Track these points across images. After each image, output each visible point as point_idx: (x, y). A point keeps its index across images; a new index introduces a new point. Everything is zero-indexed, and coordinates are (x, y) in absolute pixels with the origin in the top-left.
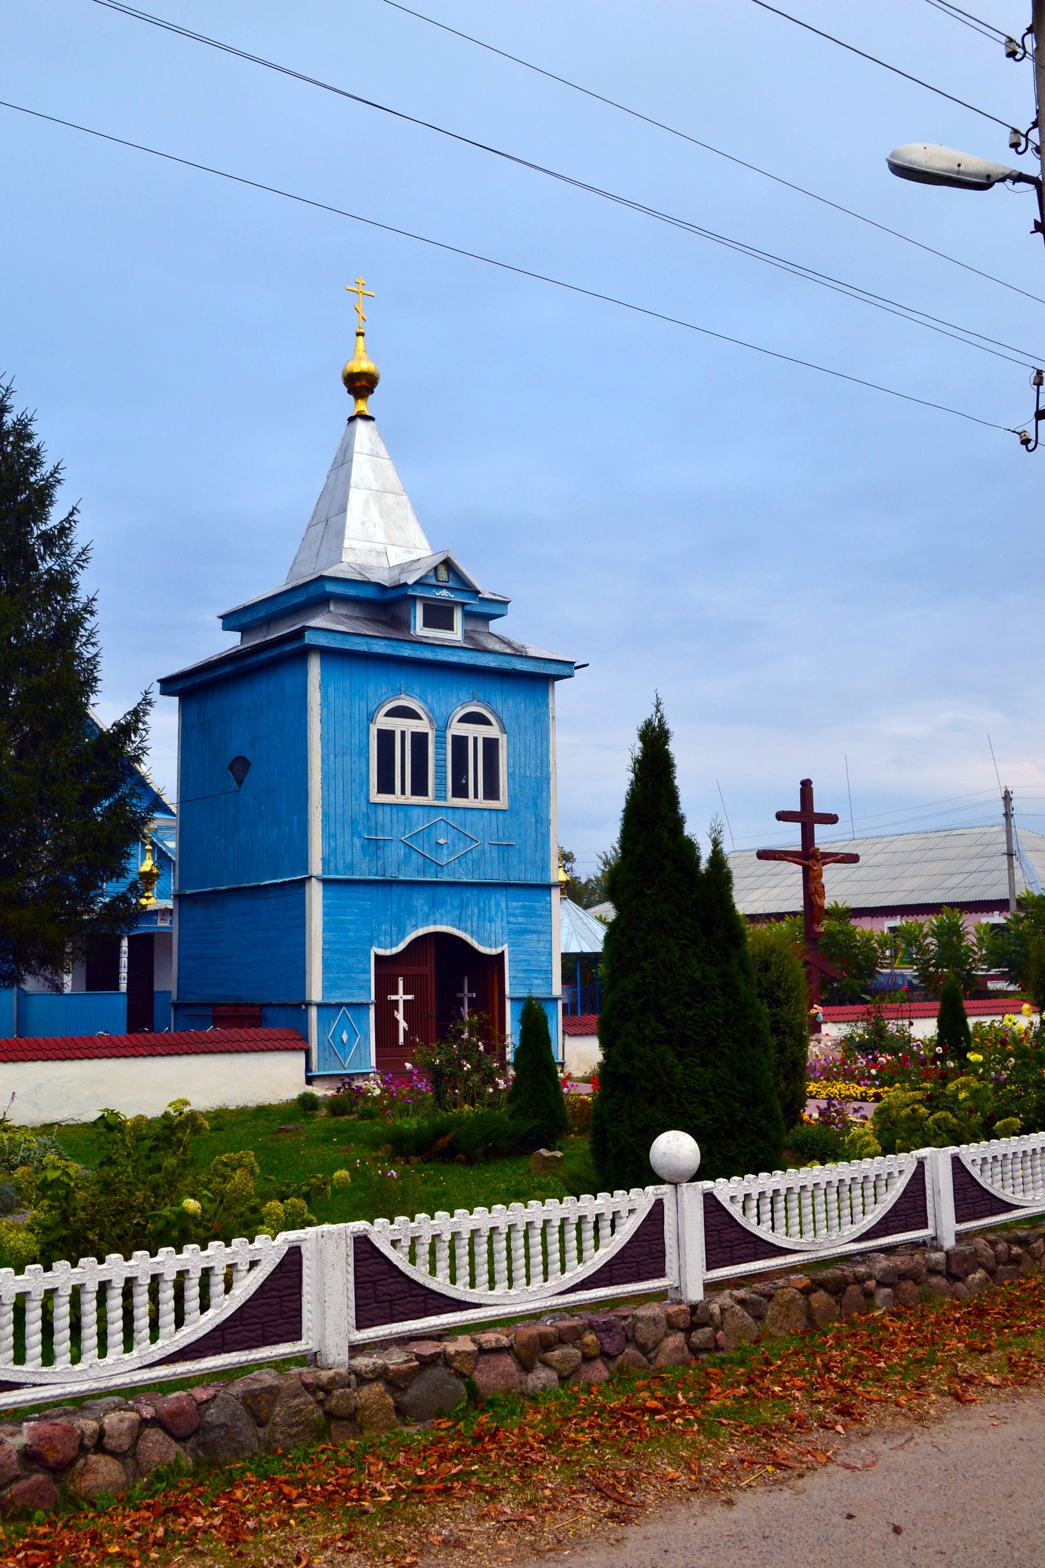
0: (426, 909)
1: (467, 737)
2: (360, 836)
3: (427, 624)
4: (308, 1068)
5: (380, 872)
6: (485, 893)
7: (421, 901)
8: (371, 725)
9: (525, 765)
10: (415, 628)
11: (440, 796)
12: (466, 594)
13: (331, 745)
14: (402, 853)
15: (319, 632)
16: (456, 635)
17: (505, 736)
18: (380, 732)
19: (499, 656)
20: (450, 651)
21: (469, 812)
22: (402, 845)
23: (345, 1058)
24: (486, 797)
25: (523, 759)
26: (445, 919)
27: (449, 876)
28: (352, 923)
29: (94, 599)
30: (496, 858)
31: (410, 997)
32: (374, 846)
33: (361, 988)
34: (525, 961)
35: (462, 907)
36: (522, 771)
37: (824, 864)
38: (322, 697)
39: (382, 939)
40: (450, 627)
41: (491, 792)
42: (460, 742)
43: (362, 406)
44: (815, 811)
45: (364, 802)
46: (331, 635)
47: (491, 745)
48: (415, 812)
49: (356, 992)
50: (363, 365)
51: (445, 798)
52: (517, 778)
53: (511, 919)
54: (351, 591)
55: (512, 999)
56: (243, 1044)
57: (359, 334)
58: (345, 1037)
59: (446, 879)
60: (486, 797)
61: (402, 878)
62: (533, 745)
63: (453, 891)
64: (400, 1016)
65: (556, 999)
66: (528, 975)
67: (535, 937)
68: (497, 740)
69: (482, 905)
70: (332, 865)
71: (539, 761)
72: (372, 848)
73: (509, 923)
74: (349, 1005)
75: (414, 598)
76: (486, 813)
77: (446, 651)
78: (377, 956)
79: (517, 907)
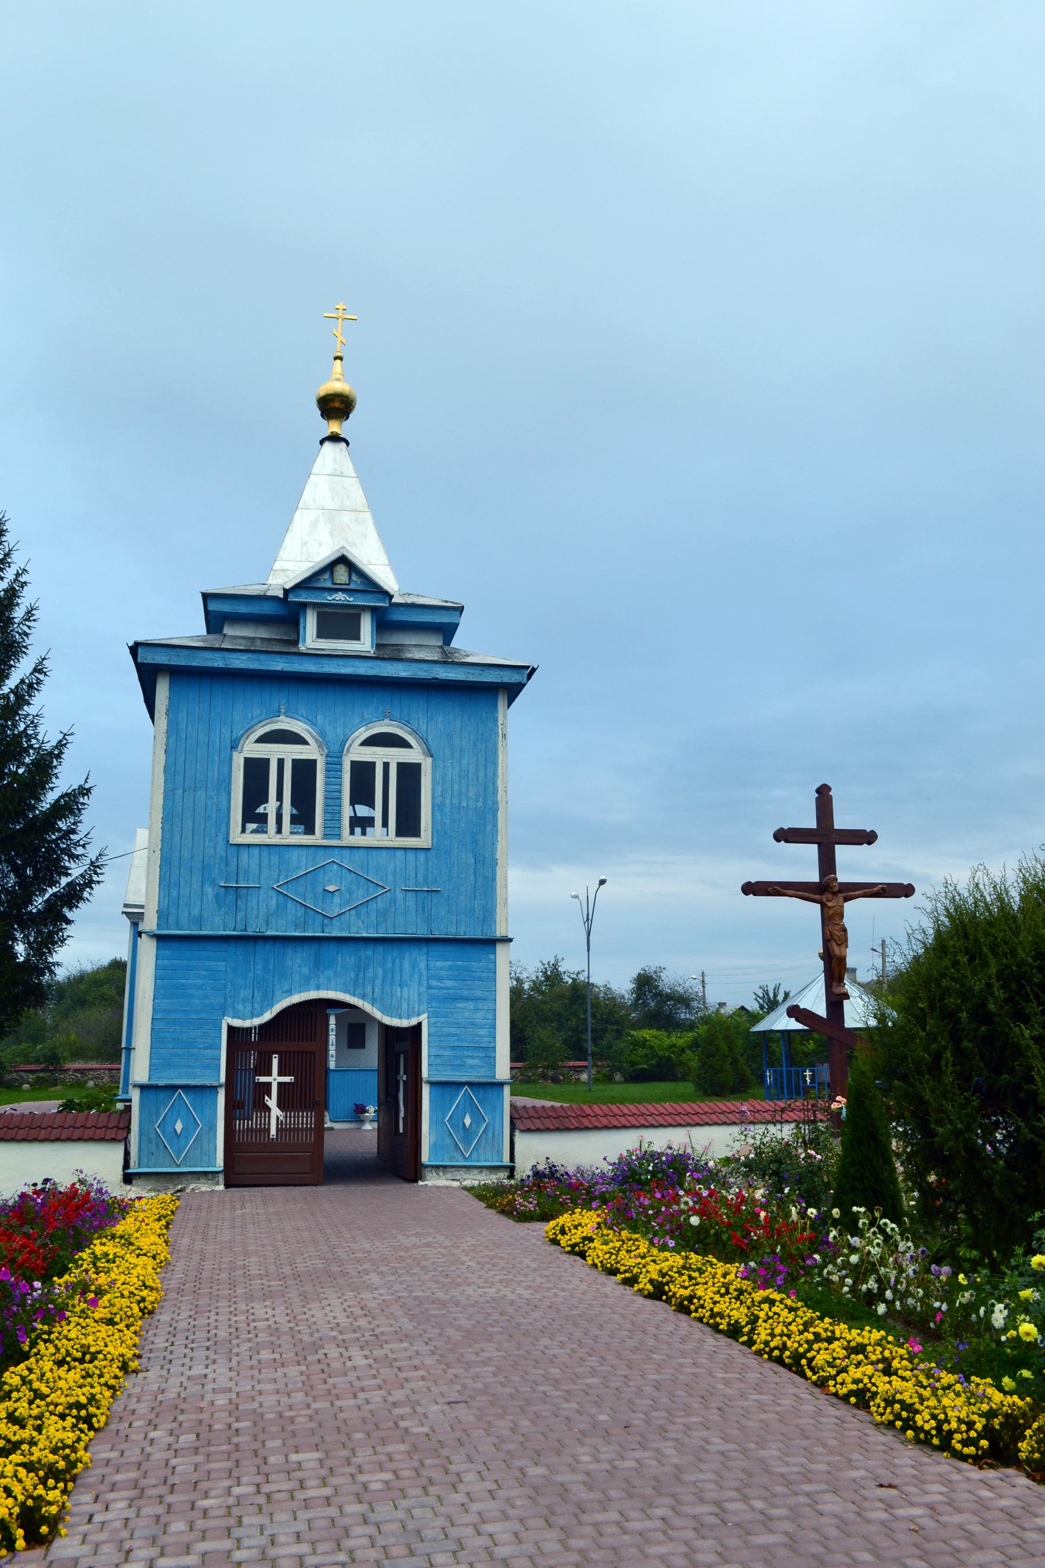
0: (305, 970)
1: (374, 763)
2: (213, 884)
3: (321, 634)
4: (126, 1165)
5: (240, 926)
6: (395, 951)
7: (299, 961)
8: (235, 754)
9: (460, 794)
10: (304, 640)
11: (332, 830)
12: (371, 596)
13: (179, 778)
14: (274, 902)
15: (159, 649)
16: (366, 642)
17: (430, 759)
18: (248, 761)
19: (412, 665)
20: (341, 662)
21: (374, 852)
22: (272, 893)
23: (179, 1153)
24: (400, 833)
25: (456, 787)
26: (333, 984)
27: (341, 930)
28: (200, 988)
29: (44, 659)
30: (413, 909)
31: (287, 1079)
32: (234, 894)
33: (207, 1067)
34: (454, 1035)
35: (360, 968)
36: (455, 801)
37: (846, 899)
38: (169, 724)
39: (240, 1007)
40: (356, 637)
41: (408, 824)
42: (363, 773)
43: (334, 427)
44: (836, 827)
45: (221, 843)
46: (174, 652)
47: (409, 774)
48: (296, 854)
49: (199, 1071)
50: (338, 386)
51: (339, 836)
52: (447, 810)
53: (434, 983)
54: (243, 609)
55: (432, 1084)
56: (704, 1117)
57: (336, 358)
58: (468, 1121)
59: (336, 933)
60: (400, 833)
61: (269, 933)
62: (472, 769)
63: (346, 948)
64: (272, 1102)
65: (501, 1085)
66: (459, 1053)
67: (471, 1005)
68: (419, 765)
69: (389, 965)
70: (172, 919)
71: (481, 789)
72: (231, 897)
73: (430, 987)
74: (186, 1088)
75: (304, 606)
76: (399, 853)
77: (335, 661)
78: (231, 1029)
79: (442, 968)
